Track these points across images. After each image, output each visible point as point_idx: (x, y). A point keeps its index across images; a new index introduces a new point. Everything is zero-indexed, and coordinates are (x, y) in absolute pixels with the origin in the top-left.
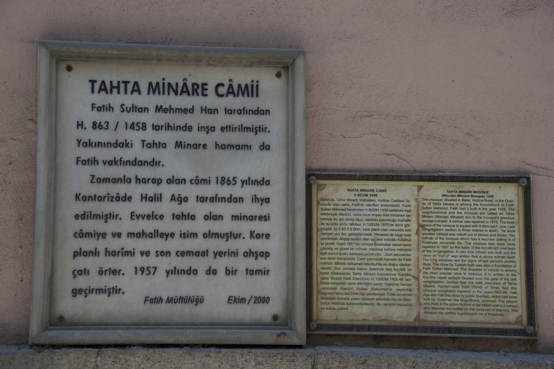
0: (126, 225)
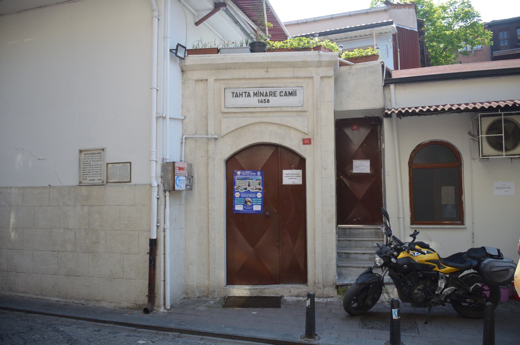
0: (87, 171)
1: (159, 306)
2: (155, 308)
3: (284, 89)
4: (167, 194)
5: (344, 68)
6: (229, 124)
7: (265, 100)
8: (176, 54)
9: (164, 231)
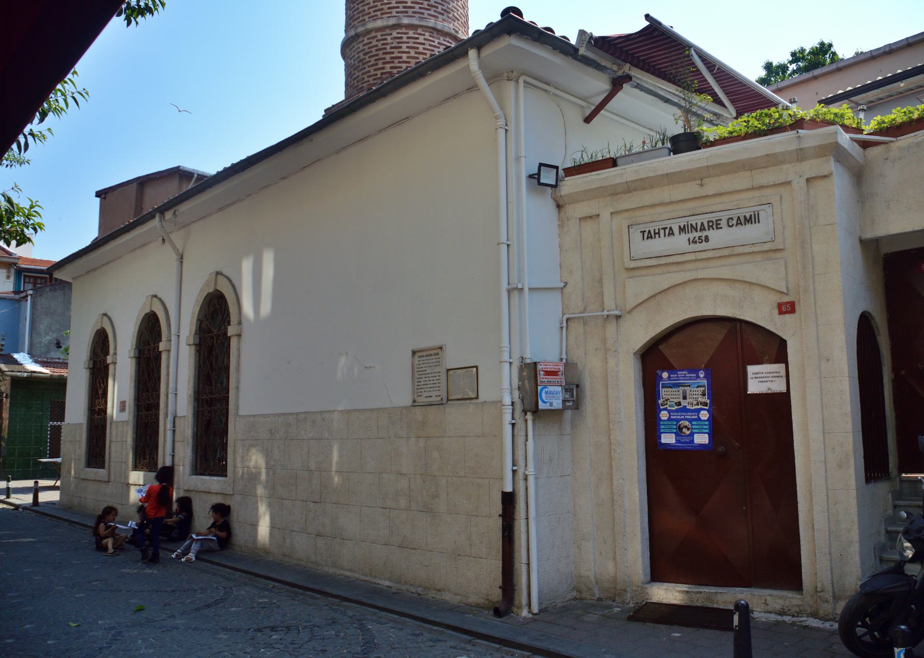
1: (520, 607)
2: (515, 609)
3: (734, 214)
4: (529, 416)
5: (873, 152)
6: (639, 288)
7: (700, 238)
8: (539, 179)
9: (526, 479)
